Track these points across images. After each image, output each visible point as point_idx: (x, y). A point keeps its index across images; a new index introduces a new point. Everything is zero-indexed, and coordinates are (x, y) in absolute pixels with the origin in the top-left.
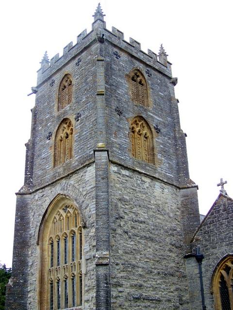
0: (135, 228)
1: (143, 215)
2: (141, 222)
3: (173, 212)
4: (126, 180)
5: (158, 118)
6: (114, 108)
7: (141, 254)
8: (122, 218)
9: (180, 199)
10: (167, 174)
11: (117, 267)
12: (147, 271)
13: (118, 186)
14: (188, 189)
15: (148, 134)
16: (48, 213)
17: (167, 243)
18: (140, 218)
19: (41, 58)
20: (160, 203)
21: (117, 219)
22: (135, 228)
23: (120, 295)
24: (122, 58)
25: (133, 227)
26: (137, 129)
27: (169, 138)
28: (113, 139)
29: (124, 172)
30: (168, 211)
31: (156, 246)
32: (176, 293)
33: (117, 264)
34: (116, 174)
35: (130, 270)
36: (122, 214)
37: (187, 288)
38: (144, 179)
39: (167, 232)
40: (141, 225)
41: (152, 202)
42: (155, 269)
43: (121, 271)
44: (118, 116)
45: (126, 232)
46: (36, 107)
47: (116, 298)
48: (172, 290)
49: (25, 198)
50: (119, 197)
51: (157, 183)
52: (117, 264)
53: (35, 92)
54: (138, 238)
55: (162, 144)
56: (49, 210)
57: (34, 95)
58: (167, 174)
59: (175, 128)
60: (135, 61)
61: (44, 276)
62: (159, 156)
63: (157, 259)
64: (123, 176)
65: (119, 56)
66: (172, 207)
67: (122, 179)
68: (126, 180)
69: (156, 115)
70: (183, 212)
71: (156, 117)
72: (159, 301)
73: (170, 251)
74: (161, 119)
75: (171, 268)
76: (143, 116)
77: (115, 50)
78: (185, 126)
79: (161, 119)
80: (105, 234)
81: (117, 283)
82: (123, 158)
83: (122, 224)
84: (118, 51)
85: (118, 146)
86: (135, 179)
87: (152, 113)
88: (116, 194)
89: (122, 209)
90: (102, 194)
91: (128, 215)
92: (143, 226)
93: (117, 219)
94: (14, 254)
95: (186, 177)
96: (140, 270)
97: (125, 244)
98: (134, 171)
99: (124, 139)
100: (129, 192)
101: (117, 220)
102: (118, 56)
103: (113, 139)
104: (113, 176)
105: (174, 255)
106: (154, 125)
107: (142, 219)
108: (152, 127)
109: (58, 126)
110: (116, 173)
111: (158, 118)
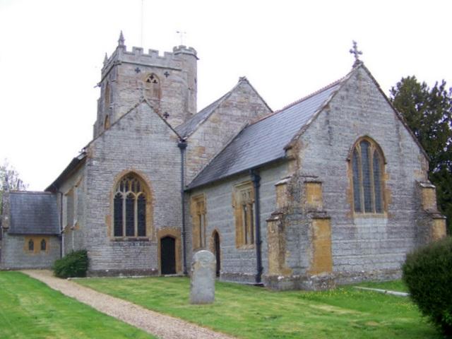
19: (103, 59)
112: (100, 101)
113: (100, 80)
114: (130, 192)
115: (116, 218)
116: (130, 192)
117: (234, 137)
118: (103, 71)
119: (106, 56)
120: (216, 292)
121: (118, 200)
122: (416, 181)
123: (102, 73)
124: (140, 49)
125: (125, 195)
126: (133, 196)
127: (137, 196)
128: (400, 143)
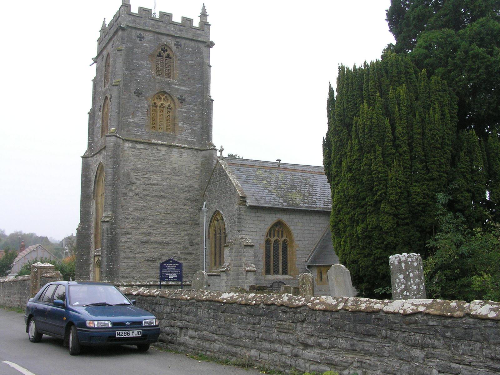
0: (147, 190)
1: (156, 178)
2: (154, 184)
3: (190, 172)
4: (141, 152)
5: (184, 88)
6: (133, 91)
7: (151, 210)
8: (133, 183)
9: (201, 160)
10: (189, 139)
11: (128, 221)
12: (156, 222)
13: (132, 158)
14: (207, 151)
15: (172, 106)
16: (98, 175)
17: (181, 198)
18: (152, 181)
19: (100, 27)
20: (177, 166)
21: (129, 185)
22: (147, 190)
23: (129, 240)
24: (146, 39)
25: (144, 190)
26: (159, 104)
27: (196, 105)
28: (130, 120)
29: (138, 146)
30: (185, 172)
31: (169, 202)
32: (187, 237)
33: (127, 219)
34: (131, 149)
35: (139, 222)
36: (134, 180)
37: (199, 233)
38: (159, 148)
39: (182, 189)
40: (154, 186)
41: (167, 166)
42: (165, 220)
43: (131, 223)
44: (137, 98)
45: (137, 194)
46: (96, 78)
47: (125, 242)
48: (182, 235)
49: (87, 161)
50: (132, 167)
51: (174, 150)
52: (127, 219)
53: (95, 62)
54: (149, 198)
55: (185, 112)
56: (98, 173)
57: (95, 64)
58: (189, 139)
59: (203, 93)
60: (160, 36)
61: (98, 223)
62: (180, 124)
63: (169, 212)
64: (138, 149)
65: (143, 38)
66: (190, 168)
67: (136, 152)
68: (141, 152)
69: (183, 86)
70: (201, 171)
71: (181, 88)
72: (168, 243)
73: (184, 205)
74: (187, 89)
75: (184, 218)
76: (166, 90)
77: (139, 32)
78: (214, 92)
79: (187, 89)
80: (110, 199)
81: (126, 232)
82: (139, 134)
83: (133, 188)
84: (142, 33)
85: (134, 125)
86: (150, 150)
87: (177, 85)
88: (126, 168)
89: (135, 177)
90: (109, 170)
91: (140, 180)
92: (155, 187)
93: (129, 185)
94: (81, 206)
95: (207, 140)
96: (150, 221)
97: (136, 203)
98: (150, 144)
99: (141, 117)
100: (143, 162)
101: (129, 186)
102: (141, 37)
103: (130, 120)
104: (128, 152)
105: (187, 208)
106: (178, 96)
107: (155, 182)
108: (175, 99)
109: (103, 101)
110: (131, 148)
111: (184, 88)
112: (95, 82)
113: (95, 55)
114: (276, 238)
115: (286, 258)
116: (276, 238)
117: (172, 97)
118: (100, 41)
119: (104, 22)
120: (462, 320)
121: (268, 242)
122: (365, 63)
123: (99, 44)
124: (149, 11)
125: (273, 240)
126: (270, 241)
127: (281, 240)
128: (415, 9)
